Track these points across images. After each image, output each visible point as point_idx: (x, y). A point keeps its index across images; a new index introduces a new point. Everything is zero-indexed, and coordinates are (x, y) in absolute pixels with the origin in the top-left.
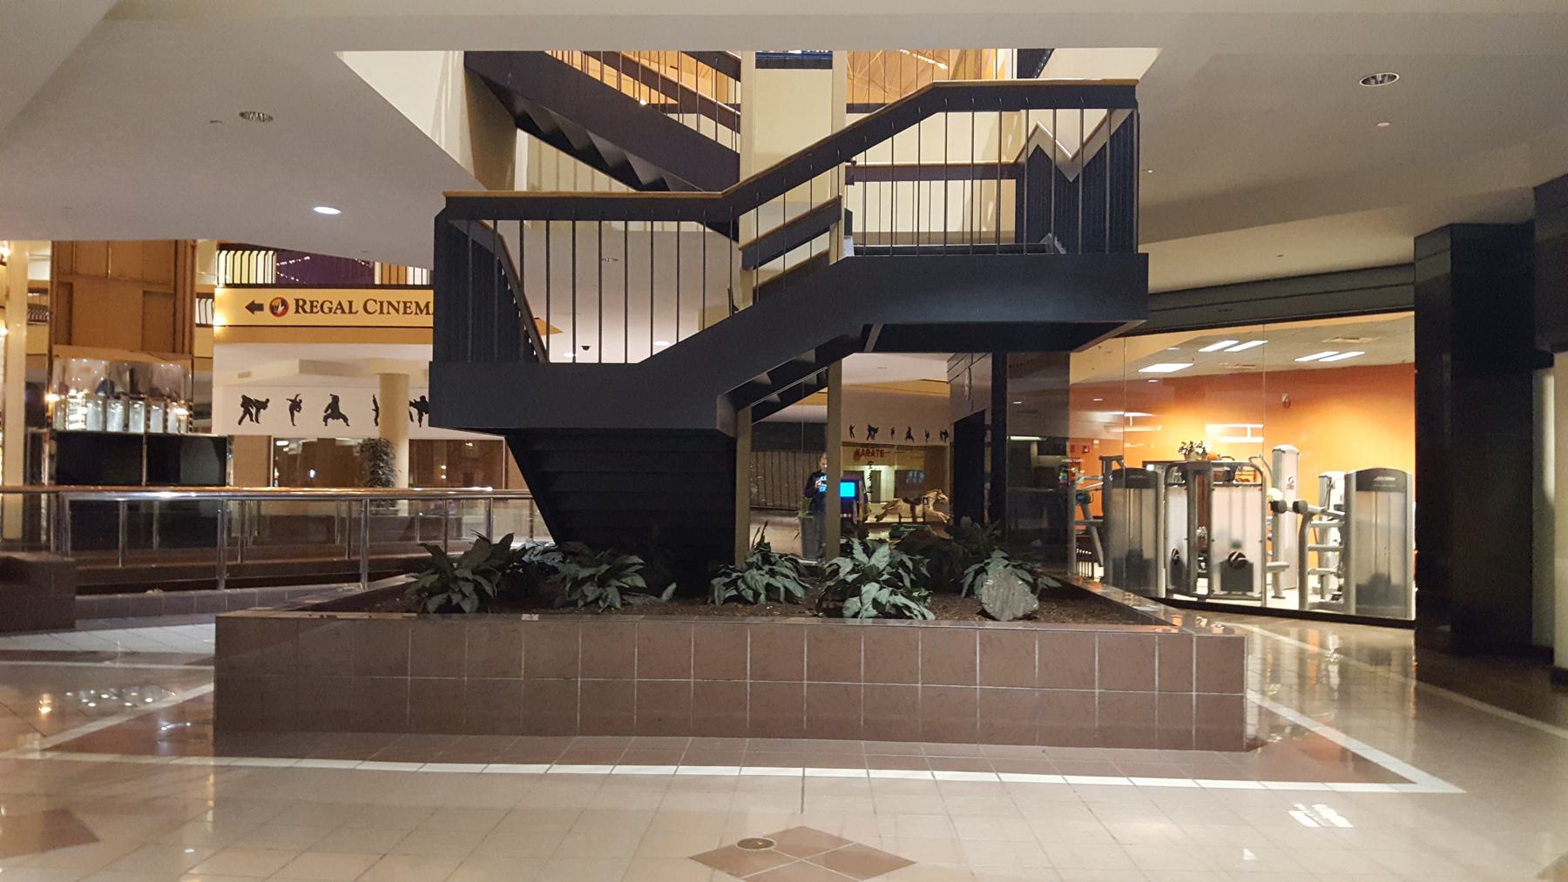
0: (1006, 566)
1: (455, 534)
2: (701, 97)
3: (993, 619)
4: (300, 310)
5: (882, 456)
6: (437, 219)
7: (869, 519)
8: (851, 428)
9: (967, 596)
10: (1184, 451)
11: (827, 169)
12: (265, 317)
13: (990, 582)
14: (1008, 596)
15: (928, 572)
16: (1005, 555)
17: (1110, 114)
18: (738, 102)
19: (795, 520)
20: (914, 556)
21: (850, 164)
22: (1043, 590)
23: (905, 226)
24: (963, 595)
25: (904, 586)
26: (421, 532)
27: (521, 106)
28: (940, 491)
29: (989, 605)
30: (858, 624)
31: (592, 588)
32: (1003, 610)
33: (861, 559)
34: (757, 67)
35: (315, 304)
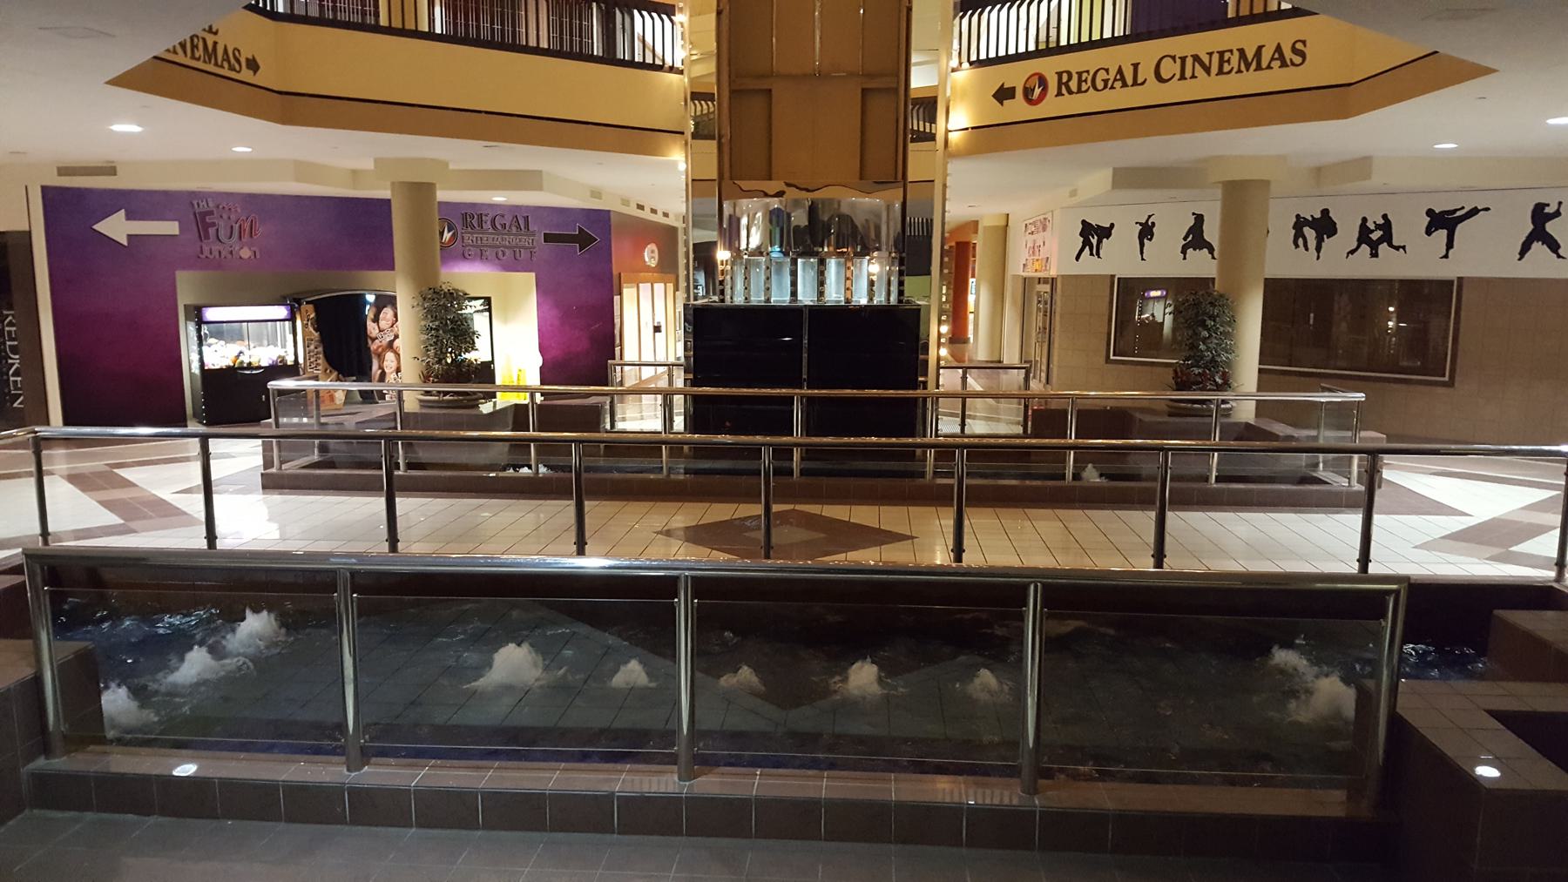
4: (1064, 91)
12: (1017, 109)
35: (1084, 76)
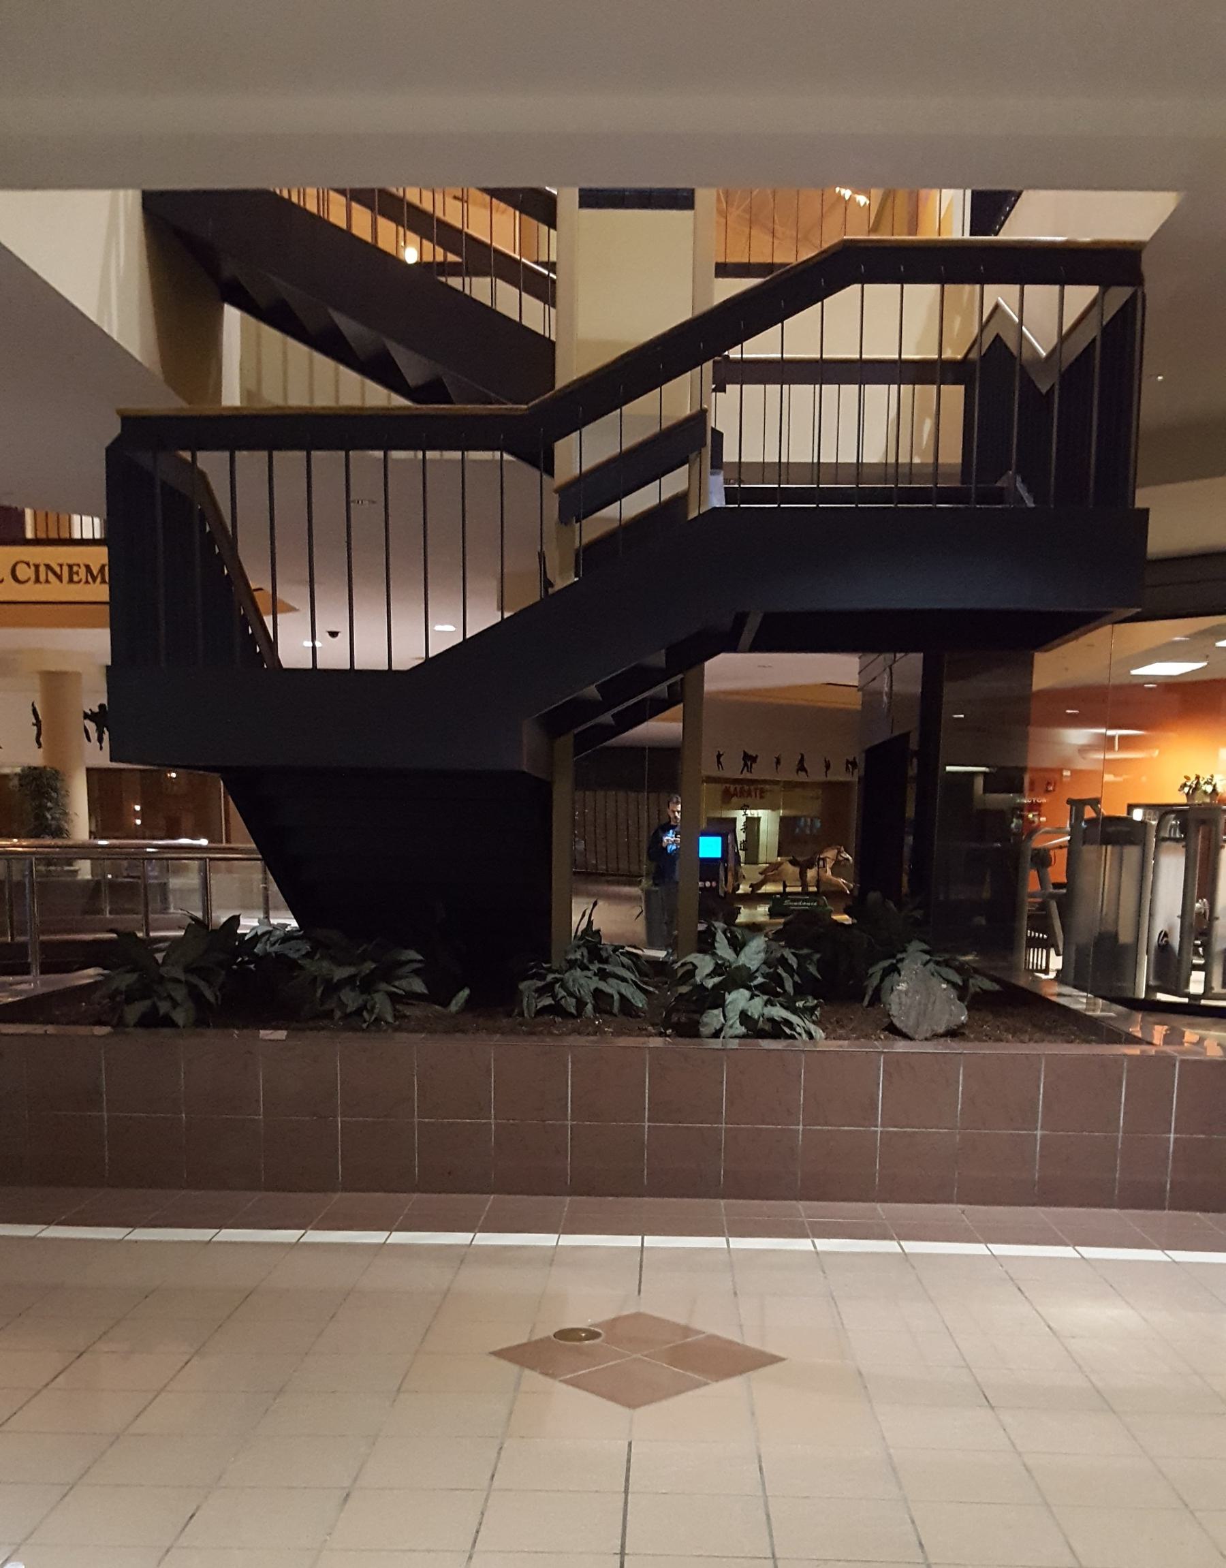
0: (925, 964)
1: (158, 905)
2: (496, 251)
3: (906, 1037)
5: (761, 797)
6: (108, 450)
7: (741, 887)
8: (719, 756)
9: (871, 1004)
10: (1186, 789)
11: (687, 371)
13: (903, 987)
14: (926, 1005)
15: (819, 973)
16: (925, 947)
17: (1102, 294)
18: (553, 258)
19: (635, 891)
20: (801, 948)
21: (719, 358)
22: (976, 994)
23: (800, 454)
24: (866, 1002)
25: (785, 991)
26: (111, 902)
27: (230, 269)
28: (842, 849)
29: (899, 1018)
30: (720, 1046)
31: (352, 994)
32: (918, 1025)
33: (725, 956)
34: (581, 206)
